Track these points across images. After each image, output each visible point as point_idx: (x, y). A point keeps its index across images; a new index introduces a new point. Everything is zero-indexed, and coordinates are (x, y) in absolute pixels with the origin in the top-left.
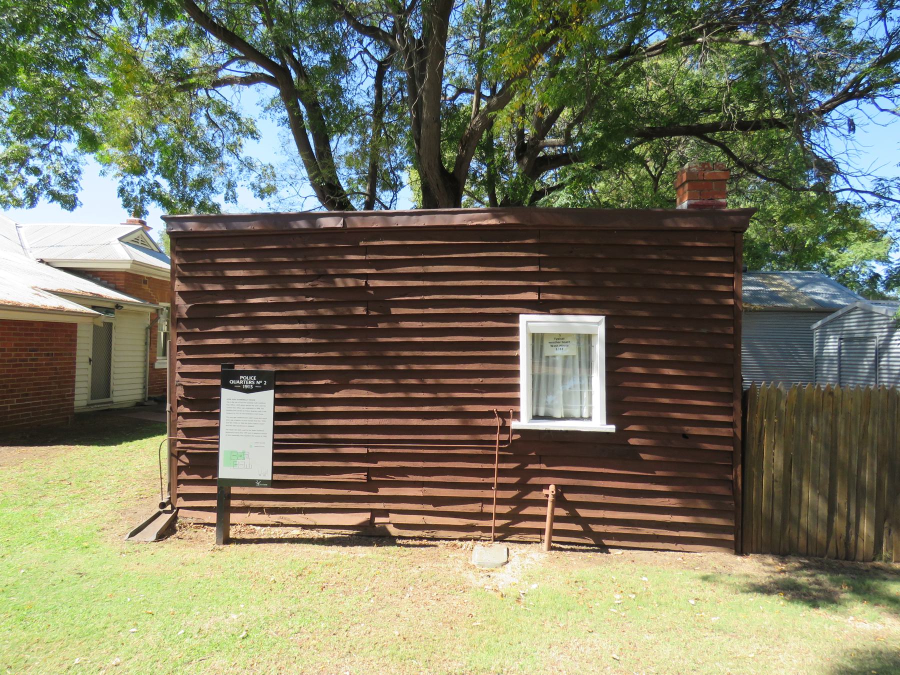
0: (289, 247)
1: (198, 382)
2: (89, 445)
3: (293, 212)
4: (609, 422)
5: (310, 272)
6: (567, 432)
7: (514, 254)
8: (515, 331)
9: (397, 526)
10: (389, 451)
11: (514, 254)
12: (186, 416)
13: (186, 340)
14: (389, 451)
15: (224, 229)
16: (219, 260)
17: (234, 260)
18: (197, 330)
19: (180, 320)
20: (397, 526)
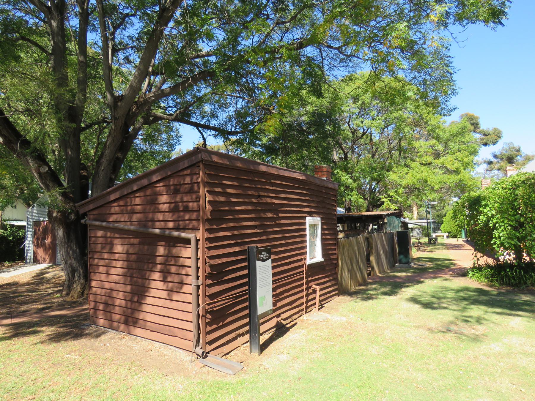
0: (251, 178)
1: (218, 261)
2: (283, 336)
3: (483, 308)
4: (323, 257)
5: (331, 232)
6: (315, 263)
7: (301, 191)
8: (304, 224)
9: (284, 320)
10: (279, 284)
11: (301, 191)
12: (209, 286)
13: (210, 234)
14: (279, 284)
15: (228, 163)
16: (225, 182)
17: (230, 183)
18: (215, 227)
19: (208, 220)
20: (284, 320)
